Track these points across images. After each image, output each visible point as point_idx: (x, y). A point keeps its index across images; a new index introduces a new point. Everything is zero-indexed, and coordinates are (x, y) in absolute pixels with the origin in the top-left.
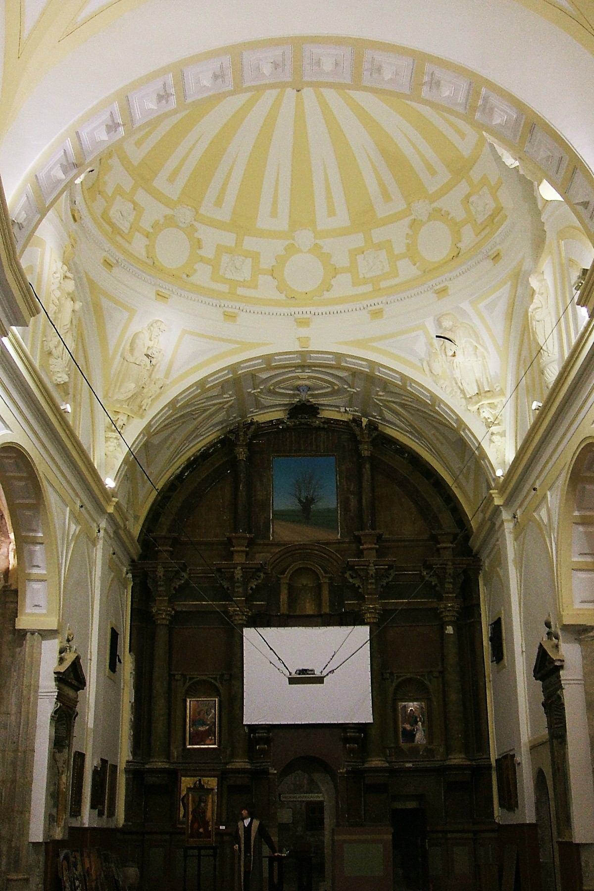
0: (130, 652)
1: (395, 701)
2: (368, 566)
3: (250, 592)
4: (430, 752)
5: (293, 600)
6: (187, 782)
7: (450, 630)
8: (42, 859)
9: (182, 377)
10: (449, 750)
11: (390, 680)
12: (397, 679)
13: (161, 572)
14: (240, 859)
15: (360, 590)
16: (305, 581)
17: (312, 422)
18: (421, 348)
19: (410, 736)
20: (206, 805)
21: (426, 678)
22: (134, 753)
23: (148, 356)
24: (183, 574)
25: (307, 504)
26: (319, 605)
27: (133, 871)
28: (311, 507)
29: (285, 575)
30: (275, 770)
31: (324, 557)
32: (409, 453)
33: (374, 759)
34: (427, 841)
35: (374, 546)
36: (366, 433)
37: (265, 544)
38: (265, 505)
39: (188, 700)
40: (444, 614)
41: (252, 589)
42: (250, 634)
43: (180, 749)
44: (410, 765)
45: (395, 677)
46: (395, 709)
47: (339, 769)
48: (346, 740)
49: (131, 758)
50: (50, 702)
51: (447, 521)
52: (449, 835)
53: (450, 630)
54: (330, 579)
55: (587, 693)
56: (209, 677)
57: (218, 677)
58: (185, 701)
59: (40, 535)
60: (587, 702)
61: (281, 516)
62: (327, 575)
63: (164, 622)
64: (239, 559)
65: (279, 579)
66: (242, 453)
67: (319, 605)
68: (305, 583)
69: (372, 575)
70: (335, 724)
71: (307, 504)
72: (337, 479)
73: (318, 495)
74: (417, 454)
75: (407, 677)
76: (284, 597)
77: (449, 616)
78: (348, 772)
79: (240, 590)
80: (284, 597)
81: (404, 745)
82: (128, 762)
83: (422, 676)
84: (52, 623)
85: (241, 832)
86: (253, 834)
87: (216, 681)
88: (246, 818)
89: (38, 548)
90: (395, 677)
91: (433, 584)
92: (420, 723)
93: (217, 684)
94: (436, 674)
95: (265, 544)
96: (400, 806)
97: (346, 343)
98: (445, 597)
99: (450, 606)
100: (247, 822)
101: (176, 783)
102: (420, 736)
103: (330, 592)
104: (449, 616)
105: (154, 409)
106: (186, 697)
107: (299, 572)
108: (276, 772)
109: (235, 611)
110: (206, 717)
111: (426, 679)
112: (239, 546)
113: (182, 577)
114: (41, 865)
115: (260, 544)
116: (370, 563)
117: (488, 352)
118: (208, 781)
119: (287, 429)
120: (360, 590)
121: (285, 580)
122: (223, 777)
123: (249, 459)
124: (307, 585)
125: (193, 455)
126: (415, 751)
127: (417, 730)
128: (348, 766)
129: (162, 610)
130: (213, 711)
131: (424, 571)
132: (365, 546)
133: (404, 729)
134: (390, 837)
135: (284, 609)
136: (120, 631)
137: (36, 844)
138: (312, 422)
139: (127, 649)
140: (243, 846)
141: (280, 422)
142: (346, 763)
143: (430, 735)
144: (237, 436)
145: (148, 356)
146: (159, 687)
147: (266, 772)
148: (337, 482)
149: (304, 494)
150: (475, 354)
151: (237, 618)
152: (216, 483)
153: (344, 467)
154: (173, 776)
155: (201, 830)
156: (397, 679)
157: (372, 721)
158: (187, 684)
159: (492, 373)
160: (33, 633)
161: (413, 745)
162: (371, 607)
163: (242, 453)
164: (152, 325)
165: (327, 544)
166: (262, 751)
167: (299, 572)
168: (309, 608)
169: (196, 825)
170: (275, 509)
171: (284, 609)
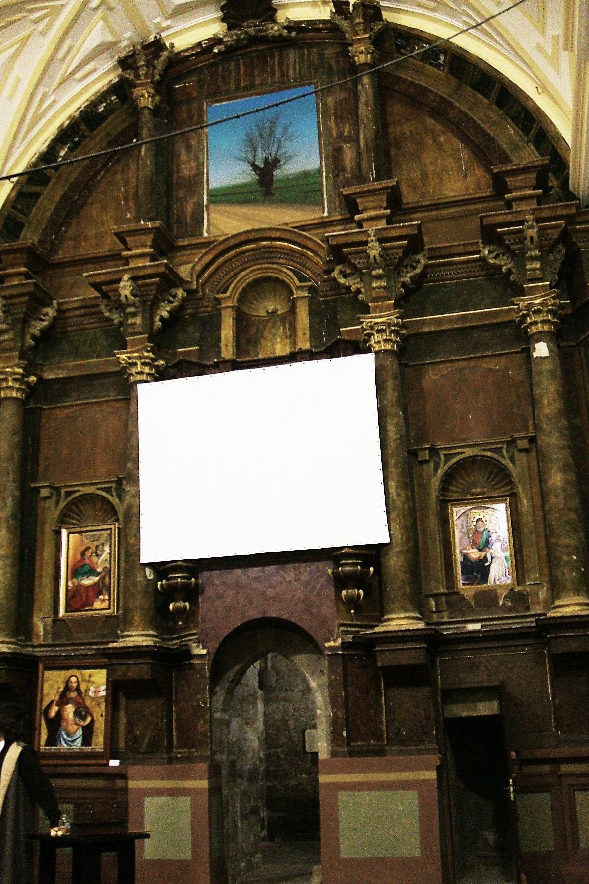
1: (444, 504)
2: (366, 243)
4: (519, 599)
7: (541, 349)
10: (556, 589)
11: (432, 464)
12: (446, 462)
16: (271, 305)
21: (505, 453)
28: (275, 173)
29: (228, 294)
30: (203, 648)
31: (295, 251)
32: (445, 52)
33: (394, 616)
34: (511, 781)
35: (382, 211)
36: (360, 23)
38: (196, 181)
39: (64, 532)
40: (529, 320)
43: (49, 621)
44: (477, 626)
45: (443, 457)
47: (329, 641)
48: (340, 582)
52: (565, 768)
53: (541, 349)
54: (311, 289)
56: (98, 489)
57: (114, 485)
58: (59, 533)
62: (303, 284)
65: (219, 301)
68: (271, 309)
69: (374, 257)
72: (318, 122)
73: (285, 153)
74: (461, 48)
75: (466, 455)
76: (227, 332)
77: (538, 324)
78: (344, 645)
79: (138, 320)
80: (227, 332)
83: (498, 451)
87: (111, 494)
90: (443, 457)
91: (504, 269)
93: (111, 499)
94: (523, 444)
96: (463, 711)
98: (526, 289)
101: (33, 686)
103: (312, 314)
104: (538, 324)
106: (61, 527)
107: (257, 287)
108: (204, 652)
110: (95, 559)
111: (503, 457)
112: (137, 247)
113: (44, 315)
115: (184, 248)
116: (369, 236)
118: (90, 676)
119: (231, 52)
120: (360, 297)
121: (229, 302)
124: (274, 313)
126: (488, 599)
127: (492, 558)
128: (347, 633)
131: (483, 248)
132: (365, 215)
133: (466, 557)
134: (432, 775)
141: (215, 41)
142: (341, 629)
147: (187, 654)
148: (319, 127)
149: (261, 155)
151: (133, 370)
152: (113, 164)
153: (330, 101)
156: (446, 462)
158: (62, 505)
165: (303, 228)
166: (180, 611)
167: (257, 287)
170: (210, 187)
171: (228, 352)
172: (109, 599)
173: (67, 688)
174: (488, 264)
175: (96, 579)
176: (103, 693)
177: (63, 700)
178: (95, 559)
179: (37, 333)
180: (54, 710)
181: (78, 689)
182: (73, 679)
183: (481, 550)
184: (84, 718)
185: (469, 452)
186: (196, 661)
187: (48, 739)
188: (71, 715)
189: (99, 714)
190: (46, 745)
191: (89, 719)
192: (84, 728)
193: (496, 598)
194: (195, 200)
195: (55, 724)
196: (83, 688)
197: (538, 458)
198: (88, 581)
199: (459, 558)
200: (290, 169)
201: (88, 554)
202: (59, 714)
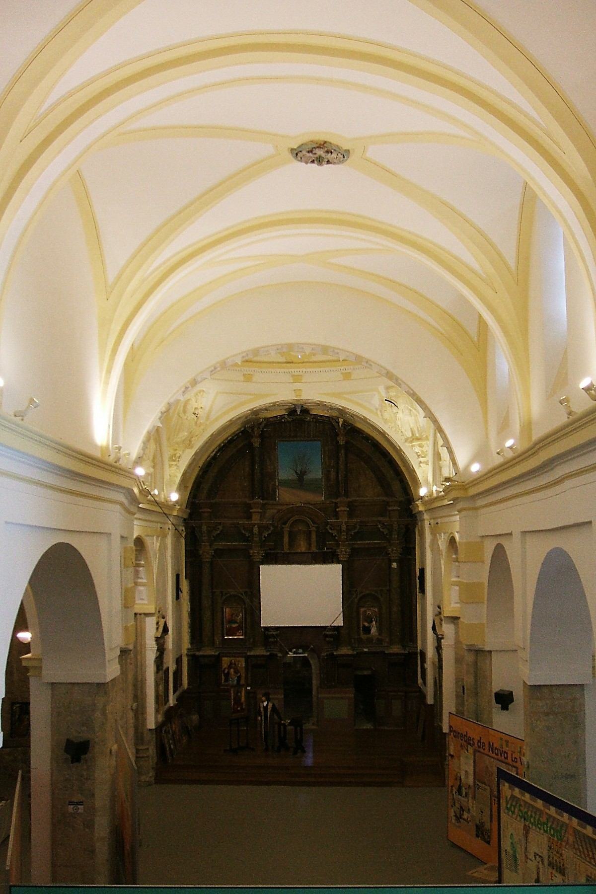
0: (186, 578)
3: (264, 539)
4: (380, 641)
5: (292, 543)
6: (226, 661)
7: (394, 565)
8: (154, 736)
9: (217, 419)
10: (391, 643)
13: (204, 528)
14: (261, 725)
15: (336, 538)
17: (305, 418)
18: (376, 401)
19: (367, 630)
20: (241, 694)
22: (191, 643)
23: (195, 414)
24: (219, 527)
25: (301, 475)
26: (310, 545)
27: (195, 718)
32: (372, 441)
37: (273, 504)
38: (273, 476)
41: (265, 537)
42: (265, 571)
46: (358, 613)
49: (190, 646)
50: (153, 653)
51: (396, 486)
53: (394, 565)
55: (456, 653)
59: (143, 563)
60: (456, 658)
61: (284, 483)
63: (208, 560)
64: (256, 519)
66: (256, 443)
67: (310, 545)
70: (319, 627)
71: (301, 475)
76: (286, 539)
78: (327, 655)
79: (257, 539)
80: (286, 539)
81: (364, 637)
82: (188, 649)
84: (151, 609)
85: (262, 709)
86: (269, 710)
88: (265, 701)
89: (141, 569)
92: (374, 622)
95: (273, 504)
96: (359, 673)
97: (328, 394)
99: (395, 551)
100: (265, 704)
102: (374, 630)
105: (198, 444)
109: (254, 553)
114: (154, 739)
117: (419, 413)
121: (286, 528)
122: (248, 658)
123: (261, 444)
125: (223, 442)
126: (370, 640)
129: (206, 551)
130: (241, 614)
133: (364, 626)
134: (353, 695)
135: (286, 549)
136: (180, 573)
137: (150, 730)
138: (305, 418)
139: (184, 578)
140: (263, 717)
143: (380, 630)
144: (253, 430)
145: (195, 414)
146: (206, 603)
149: (299, 468)
150: (410, 414)
153: (326, 448)
154: (218, 659)
155: (239, 709)
157: (342, 625)
159: (421, 425)
160: (140, 614)
161: (370, 636)
162: (343, 551)
163: (256, 443)
164: (197, 394)
168: (302, 547)
169: (236, 706)
172: (243, 632)
173: (231, 663)
174: (380, 530)
175: (237, 625)
176: (244, 666)
177: (230, 667)
178: (236, 618)
179: (215, 535)
180: (226, 672)
181: (235, 664)
182: (233, 661)
183: (368, 623)
184: (237, 673)
185: (367, 592)
186: (278, 658)
187: (225, 679)
188: (233, 673)
189: (243, 673)
190: (225, 682)
191: (239, 674)
192: (238, 677)
193: (372, 640)
194: (273, 483)
195: (227, 675)
196: (237, 664)
197: (453, 843)
198: (234, 626)
199: (362, 626)
200: (309, 476)
201: (234, 616)
202: (228, 673)
